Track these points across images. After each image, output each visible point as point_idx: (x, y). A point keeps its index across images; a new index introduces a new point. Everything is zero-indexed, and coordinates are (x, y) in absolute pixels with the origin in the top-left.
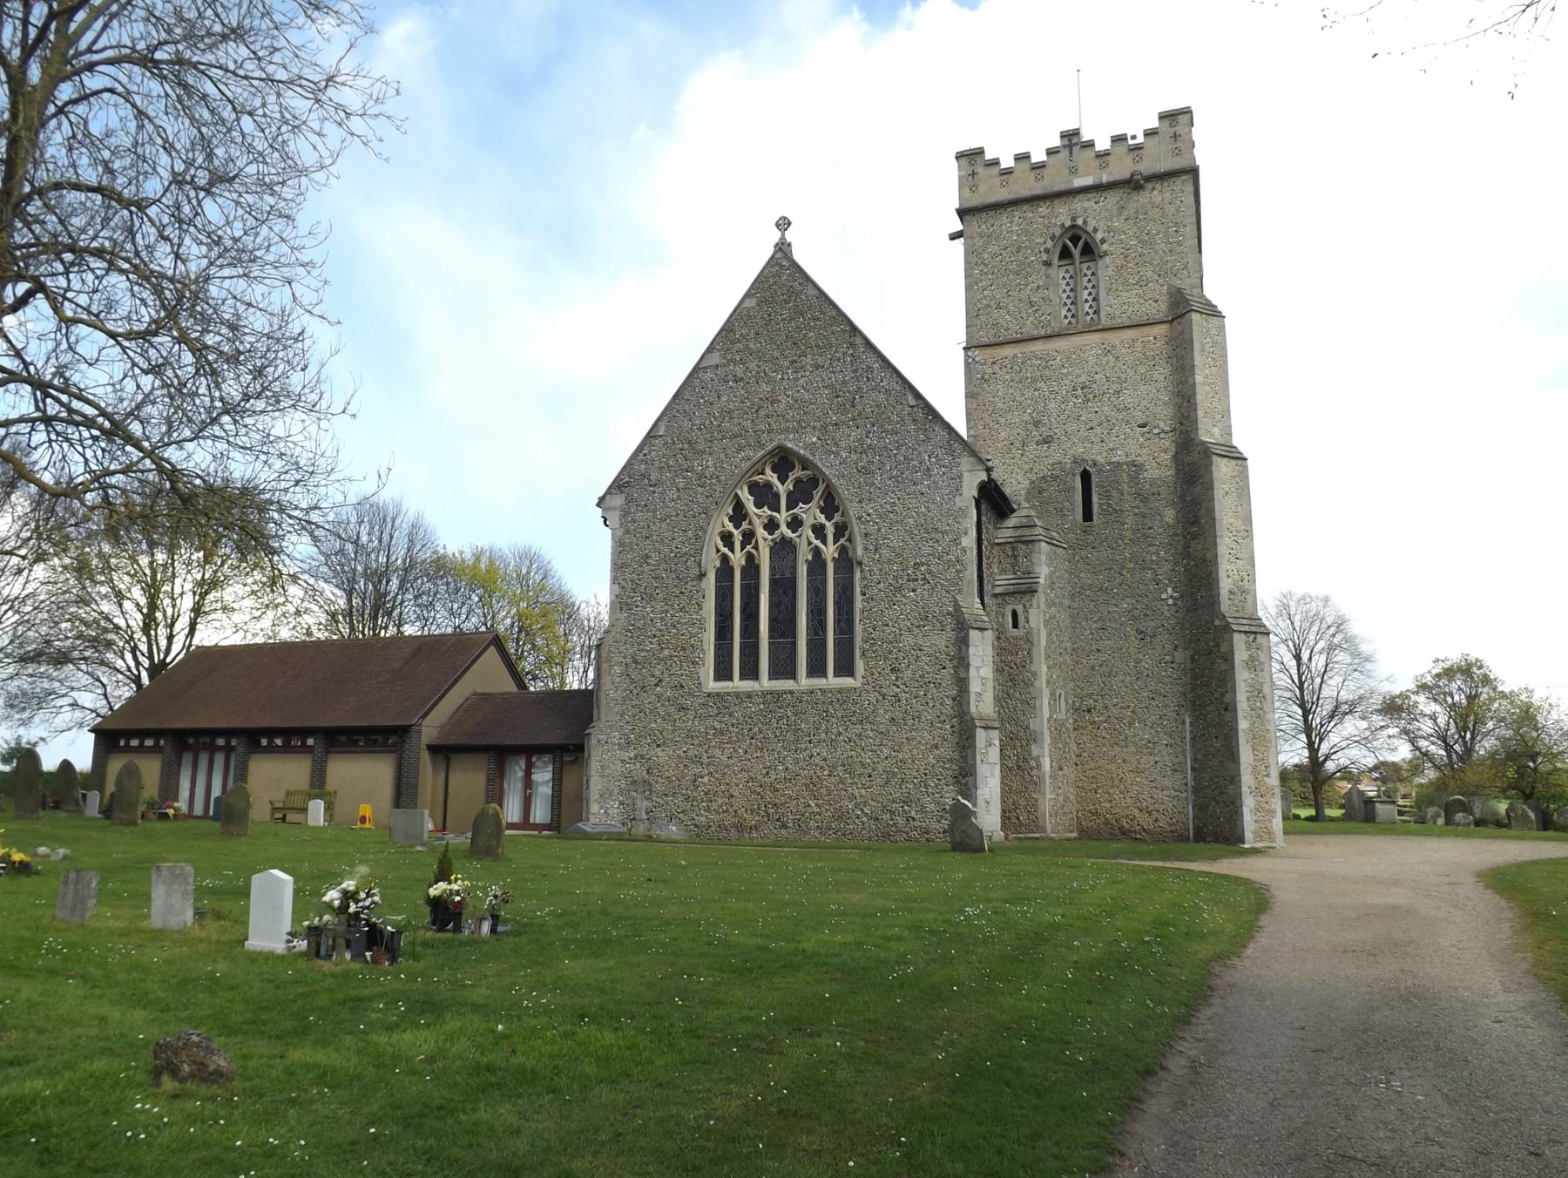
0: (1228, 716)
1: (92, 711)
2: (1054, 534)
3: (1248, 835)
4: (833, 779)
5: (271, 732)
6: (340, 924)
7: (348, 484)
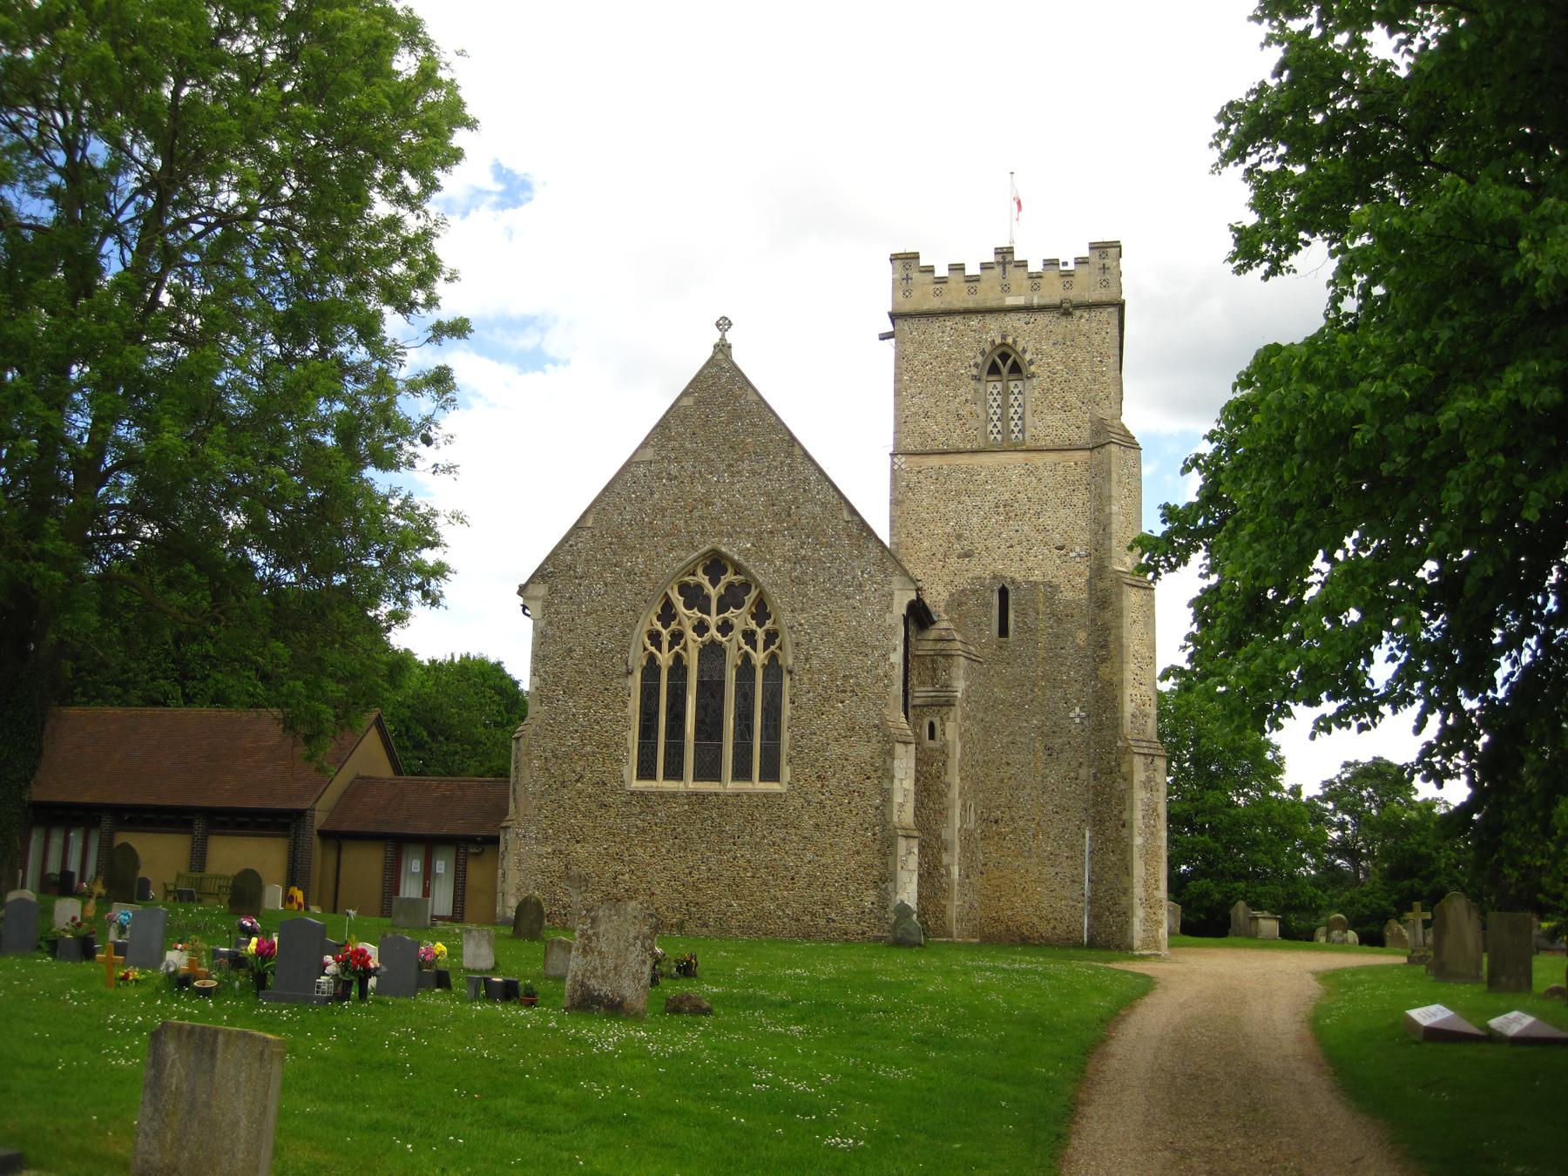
0: (1125, 832)
2: (971, 648)
3: (1137, 943)
4: (756, 881)
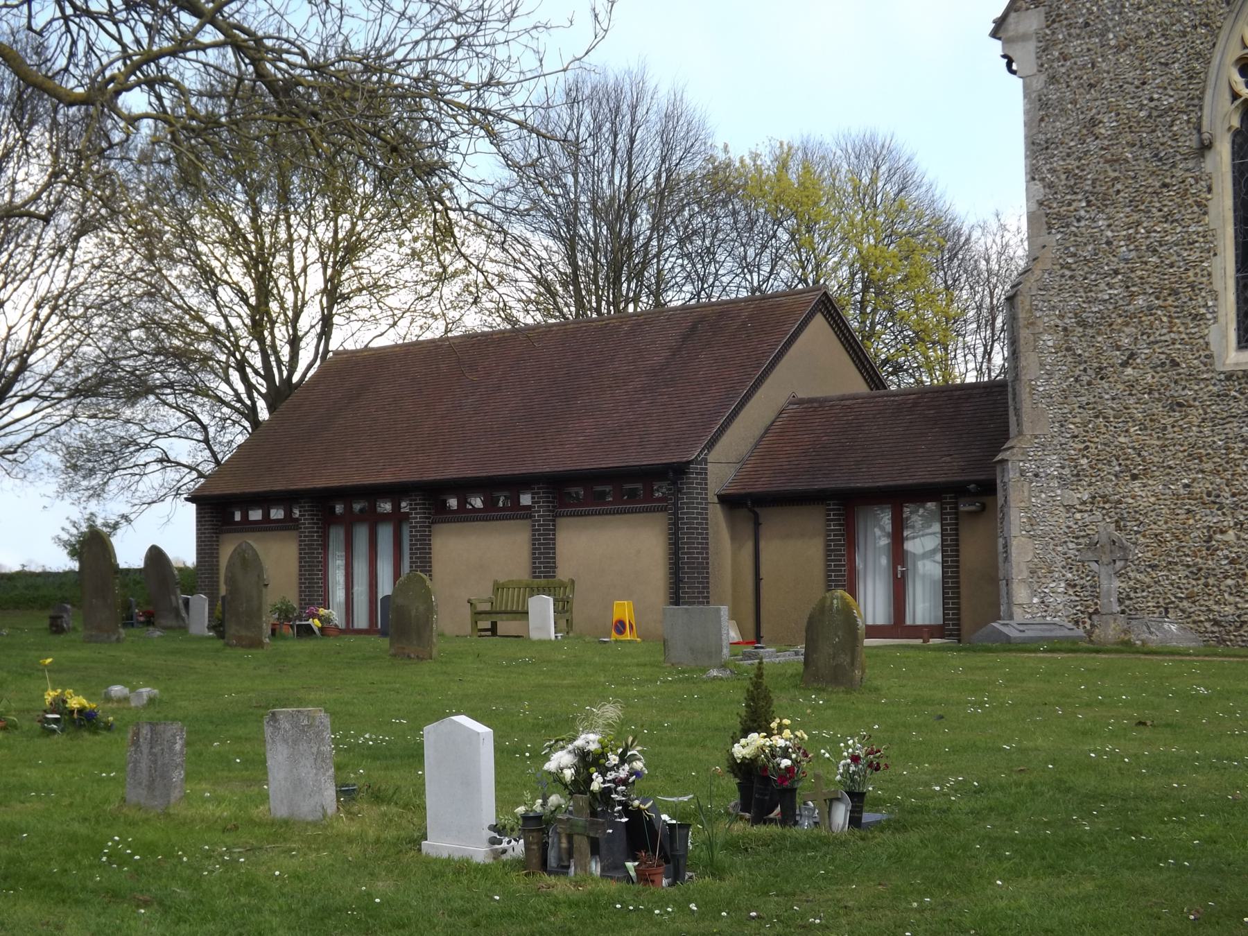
1: (191, 468)
5: (463, 487)
6: (578, 811)
7: (543, 35)
